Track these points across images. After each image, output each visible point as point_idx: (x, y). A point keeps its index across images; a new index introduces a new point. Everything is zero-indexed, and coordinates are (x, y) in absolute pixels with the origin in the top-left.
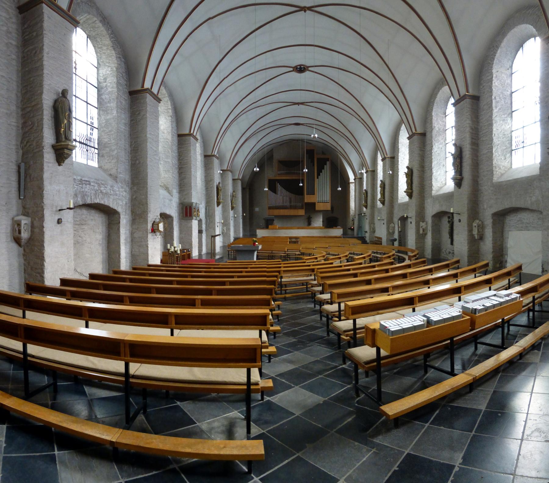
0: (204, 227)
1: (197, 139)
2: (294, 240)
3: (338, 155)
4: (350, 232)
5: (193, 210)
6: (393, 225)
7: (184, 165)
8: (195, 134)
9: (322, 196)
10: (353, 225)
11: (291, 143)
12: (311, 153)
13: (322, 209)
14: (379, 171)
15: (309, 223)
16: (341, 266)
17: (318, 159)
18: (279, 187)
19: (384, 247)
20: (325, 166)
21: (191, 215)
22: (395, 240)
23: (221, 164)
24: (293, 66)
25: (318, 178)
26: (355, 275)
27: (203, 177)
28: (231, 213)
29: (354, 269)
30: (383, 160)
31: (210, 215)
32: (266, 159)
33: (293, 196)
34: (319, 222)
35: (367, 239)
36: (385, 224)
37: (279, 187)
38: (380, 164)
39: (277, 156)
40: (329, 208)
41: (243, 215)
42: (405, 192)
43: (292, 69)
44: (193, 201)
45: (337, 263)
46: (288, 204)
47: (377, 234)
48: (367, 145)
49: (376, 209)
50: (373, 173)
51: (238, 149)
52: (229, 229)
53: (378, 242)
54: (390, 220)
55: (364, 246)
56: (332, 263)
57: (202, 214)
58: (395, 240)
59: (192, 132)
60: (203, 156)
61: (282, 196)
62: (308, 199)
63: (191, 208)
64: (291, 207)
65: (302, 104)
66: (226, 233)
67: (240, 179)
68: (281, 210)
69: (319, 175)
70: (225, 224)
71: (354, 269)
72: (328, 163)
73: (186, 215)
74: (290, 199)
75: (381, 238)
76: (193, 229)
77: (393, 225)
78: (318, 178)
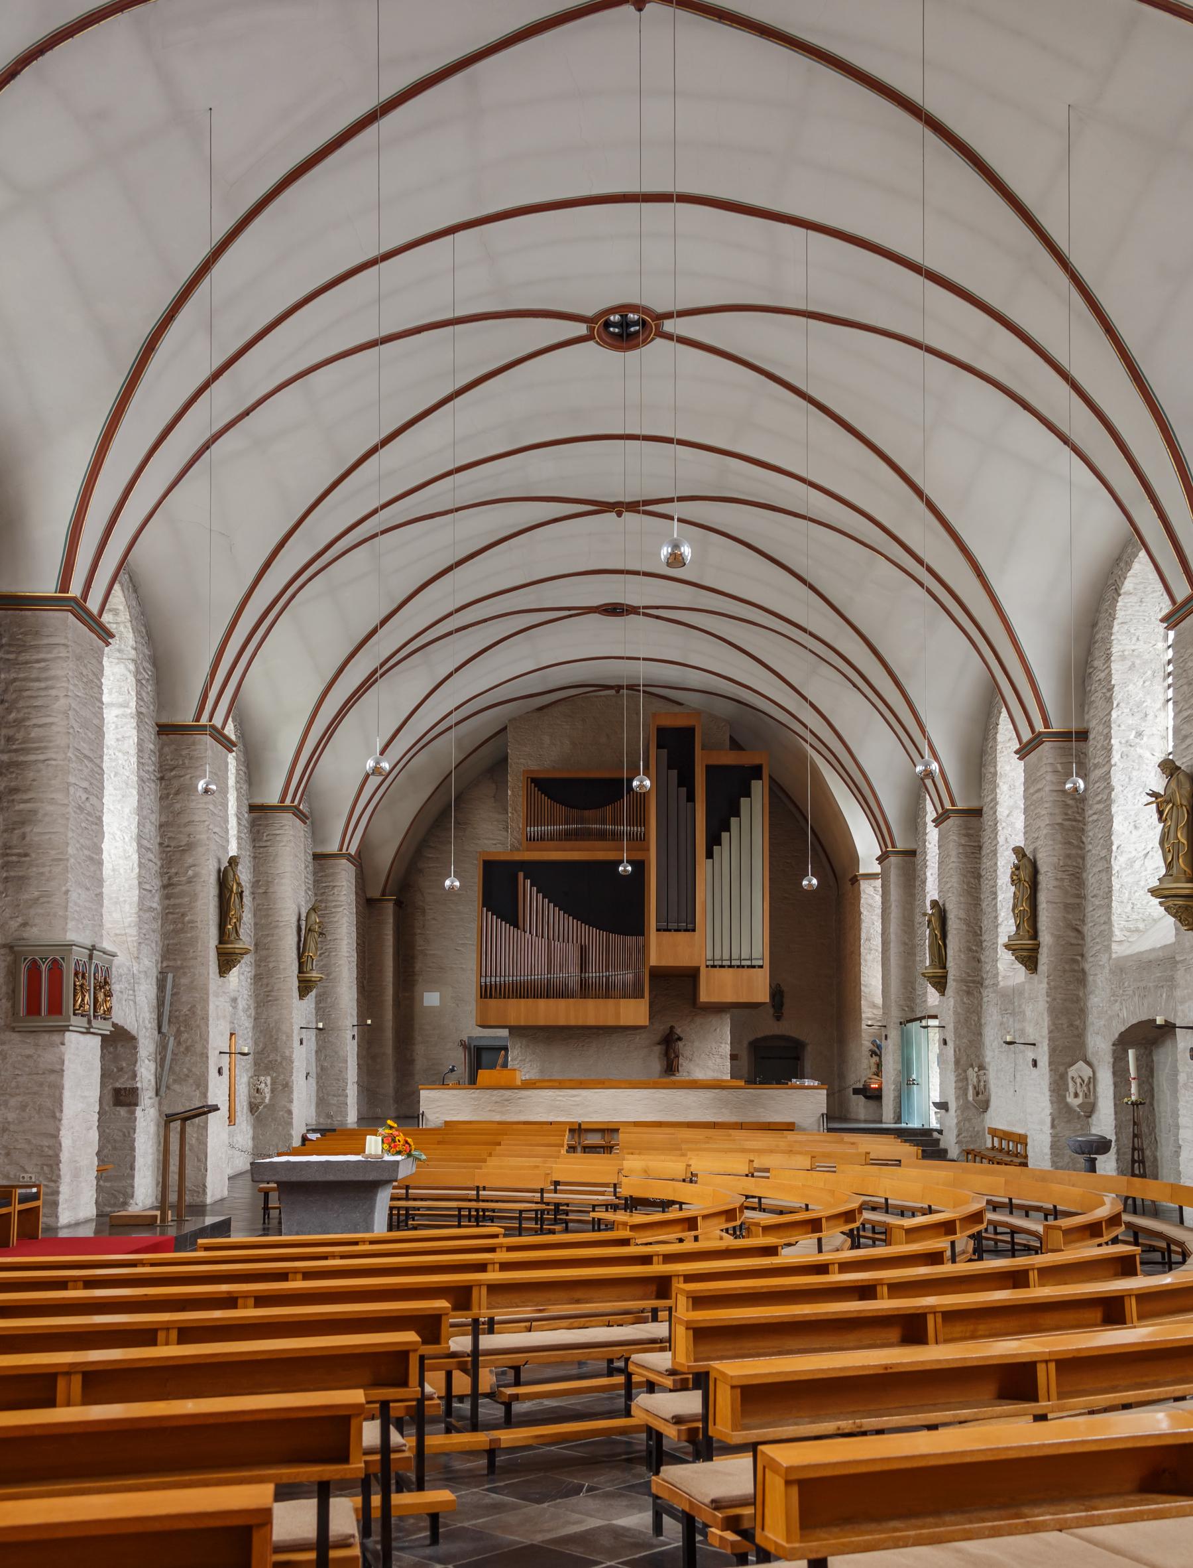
0: (146, 1072)
1: (106, 635)
2: (594, 1139)
3: (805, 755)
4: (860, 1107)
5: (69, 980)
6: (1087, 1072)
7: (26, 751)
8: (93, 605)
9: (730, 930)
10: (878, 1073)
11: (586, 701)
12: (676, 745)
13: (730, 998)
14: (1002, 811)
15: (669, 1061)
16: (822, 1269)
17: (710, 769)
18: (531, 898)
19: (1042, 1177)
20: (744, 802)
21: (56, 1008)
22: (1103, 1146)
23: (252, 771)
24: (590, 312)
25: (710, 855)
26: (912, 1329)
27: (151, 830)
28: (299, 1012)
29: (897, 1288)
30: (1024, 752)
31: (178, 1015)
32: (477, 770)
33: (595, 937)
34: (712, 1054)
35: (950, 1142)
36: (1044, 1062)
37: (531, 898)
38: (1010, 774)
39: (527, 759)
40: (762, 994)
41: (361, 1024)
42: (1154, 892)
43: (581, 329)
44: (71, 936)
45: (802, 1250)
46: (571, 975)
47: (1000, 1117)
48: (941, 676)
49: (989, 996)
50: (972, 821)
51: (346, 720)
52: (283, 1088)
53: (1010, 1151)
54: (1068, 1046)
55: (937, 1172)
56: (771, 1251)
57: (134, 1007)
58: (1103, 1146)
59: (75, 590)
60: (153, 730)
61: (546, 940)
62: (663, 949)
63: (56, 969)
64: (585, 990)
65: (633, 507)
66: (271, 1107)
67: (349, 857)
68: (542, 1003)
69: (714, 840)
70: (268, 1057)
71: (897, 1288)
72: (757, 787)
73: (33, 1008)
74: (583, 951)
75: (1022, 1140)
76: (68, 1082)
77: (1087, 1072)
78: (710, 855)
